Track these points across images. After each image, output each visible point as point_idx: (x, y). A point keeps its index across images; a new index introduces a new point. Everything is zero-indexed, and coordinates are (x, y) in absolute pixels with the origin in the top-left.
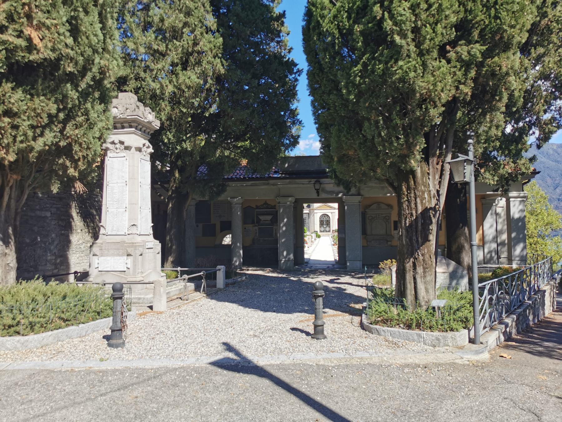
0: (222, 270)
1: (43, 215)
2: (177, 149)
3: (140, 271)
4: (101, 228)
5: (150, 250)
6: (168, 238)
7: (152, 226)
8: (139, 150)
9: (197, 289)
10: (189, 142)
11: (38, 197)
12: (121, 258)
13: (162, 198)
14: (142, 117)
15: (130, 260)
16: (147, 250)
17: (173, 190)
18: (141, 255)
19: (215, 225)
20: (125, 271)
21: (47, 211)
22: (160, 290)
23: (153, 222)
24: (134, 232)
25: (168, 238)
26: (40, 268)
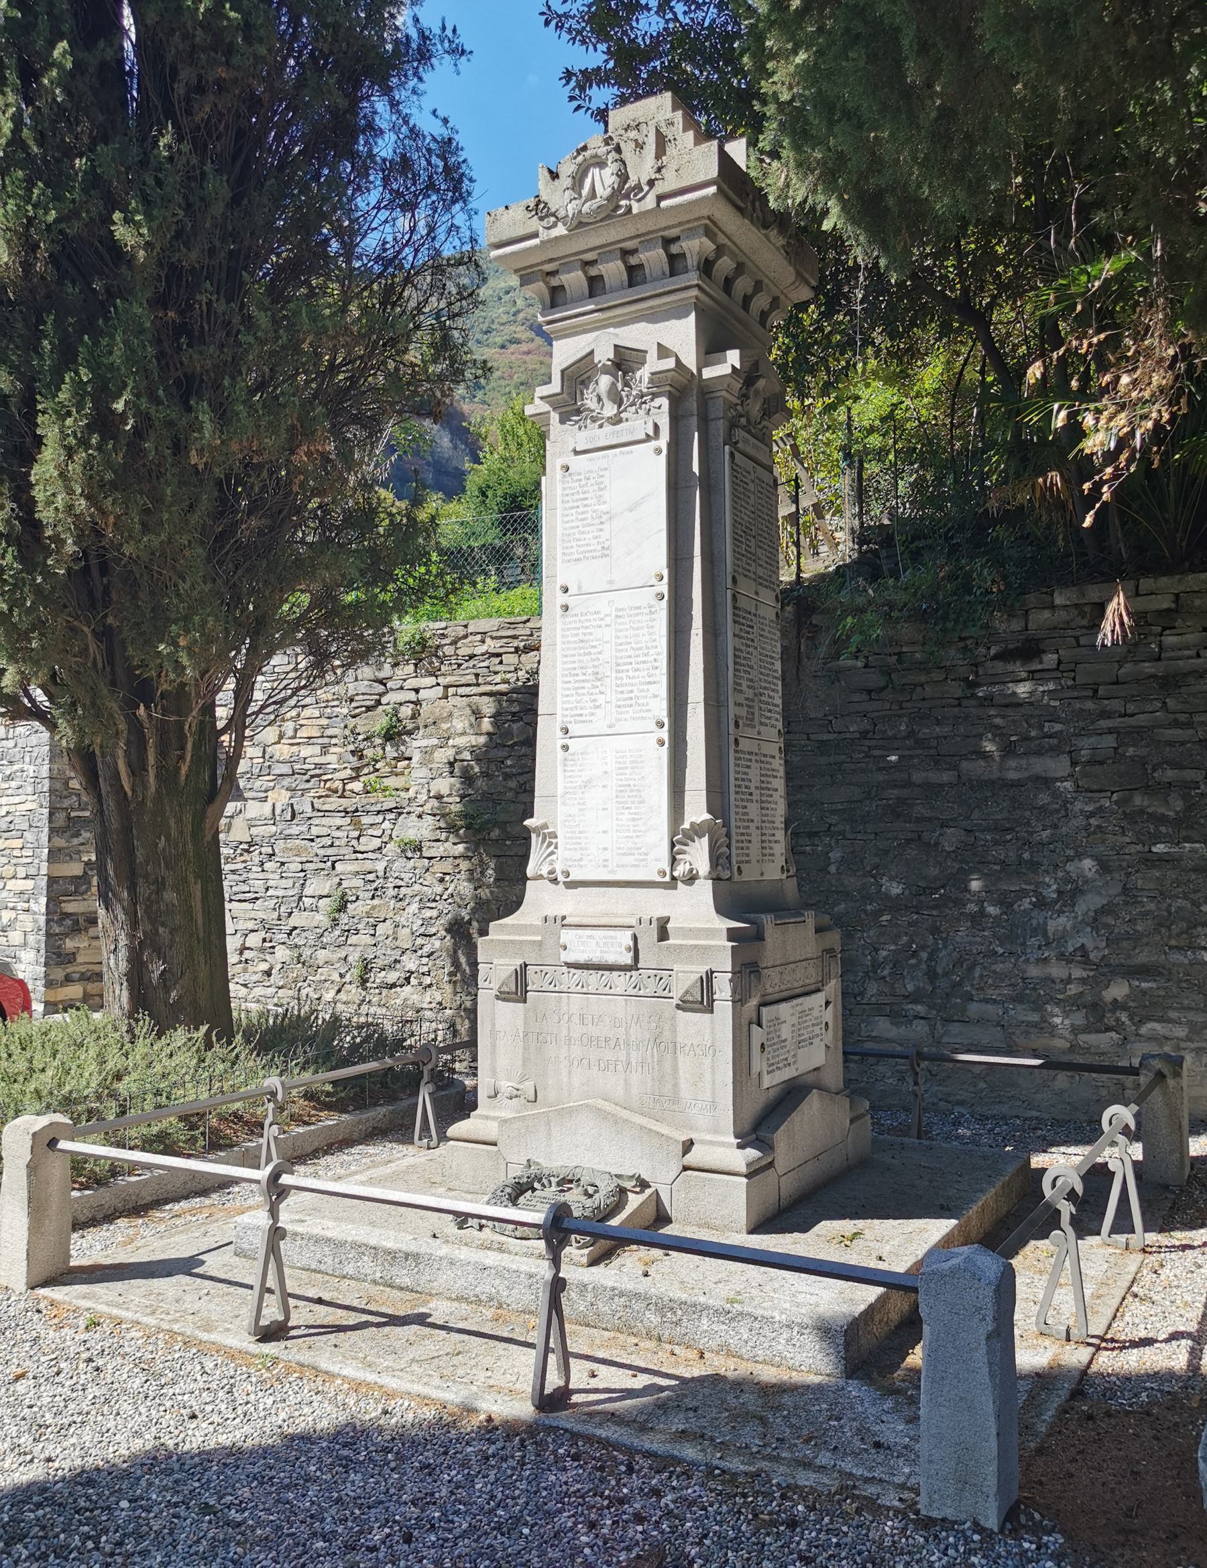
1: (1012, 775)
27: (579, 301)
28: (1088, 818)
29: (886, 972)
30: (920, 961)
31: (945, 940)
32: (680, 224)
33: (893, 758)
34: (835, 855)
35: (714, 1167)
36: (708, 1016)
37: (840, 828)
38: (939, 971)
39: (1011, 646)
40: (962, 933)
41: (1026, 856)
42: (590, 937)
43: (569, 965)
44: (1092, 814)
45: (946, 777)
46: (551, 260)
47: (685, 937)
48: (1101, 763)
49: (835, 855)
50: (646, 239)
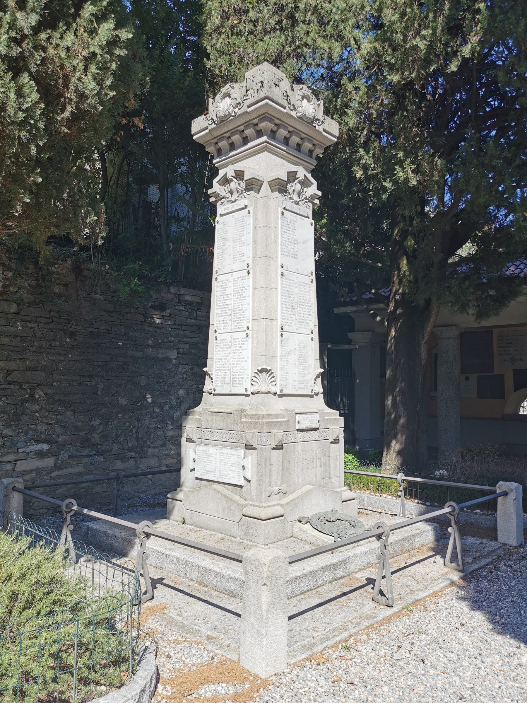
0: (512, 496)
1: (161, 356)
2: (385, 189)
3: (276, 489)
4: (207, 378)
5: (308, 434)
6: (389, 401)
7: (322, 375)
8: (280, 186)
9: (439, 548)
10: (412, 163)
11: (152, 324)
12: (233, 452)
13: (378, 319)
14: (285, 103)
15: (250, 460)
16: (300, 435)
17: (396, 301)
18: (279, 447)
19: (502, 377)
20: (241, 487)
21: (168, 348)
22: (259, 598)
23: (322, 365)
24: (264, 389)
25: (389, 401)
26: (150, 451)
27: (279, 142)
28: (183, 374)
29: (122, 439)
30: (133, 434)
31: (141, 423)
32: (320, 142)
33: (120, 344)
34: (100, 386)
35: (350, 499)
36: (281, 450)
37: (101, 374)
38: (140, 437)
39: (156, 304)
40: (147, 421)
41: (166, 388)
42: (307, 417)
43: (299, 430)
44: (184, 373)
45: (139, 354)
46: (280, 120)
47: (329, 416)
48: (186, 354)
49: (100, 386)
50: (310, 139)
